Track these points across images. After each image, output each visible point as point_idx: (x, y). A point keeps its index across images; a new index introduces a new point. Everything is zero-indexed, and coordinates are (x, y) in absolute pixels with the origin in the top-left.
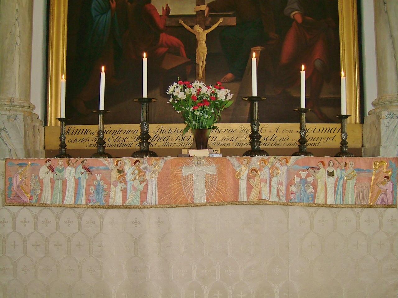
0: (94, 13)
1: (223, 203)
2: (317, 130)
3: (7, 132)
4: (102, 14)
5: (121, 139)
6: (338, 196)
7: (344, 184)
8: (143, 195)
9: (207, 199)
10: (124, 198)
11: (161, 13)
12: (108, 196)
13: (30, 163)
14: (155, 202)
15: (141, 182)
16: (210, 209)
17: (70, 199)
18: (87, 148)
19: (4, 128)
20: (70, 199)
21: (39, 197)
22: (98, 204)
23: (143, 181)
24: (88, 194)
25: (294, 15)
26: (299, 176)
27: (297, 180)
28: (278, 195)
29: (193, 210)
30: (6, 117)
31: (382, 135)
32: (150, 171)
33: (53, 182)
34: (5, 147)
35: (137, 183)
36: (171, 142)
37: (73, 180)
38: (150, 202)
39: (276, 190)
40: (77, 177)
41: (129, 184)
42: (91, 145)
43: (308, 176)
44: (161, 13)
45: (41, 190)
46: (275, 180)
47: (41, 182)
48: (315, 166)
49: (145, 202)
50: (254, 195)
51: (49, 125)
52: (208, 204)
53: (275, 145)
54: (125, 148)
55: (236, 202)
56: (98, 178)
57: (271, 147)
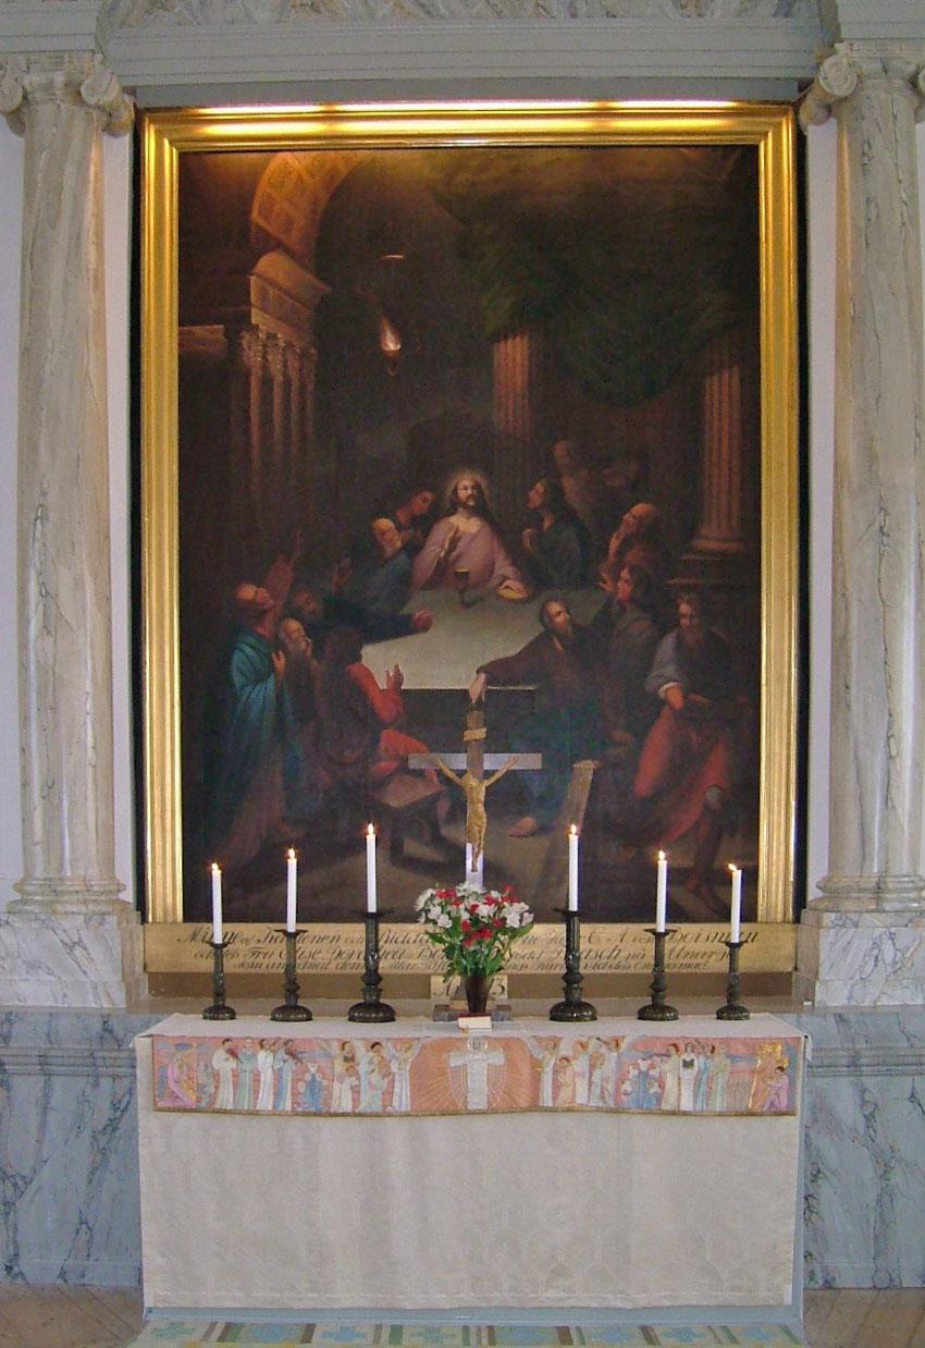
0: (238, 679)
1: (513, 1110)
2: (704, 937)
3: (85, 949)
4: (257, 683)
5: (307, 954)
6: (700, 1098)
7: (711, 1079)
8: (387, 1097)
9: (489, 1103)
10: (356, 1101)
11: (382, 685)
12: (330, 1096)
13: (195, 1045)
14: (405, 1106)
15: (384, 1076)
16: (491, 1119)
17: (265, 1102)
18: (237, 971)
19: (80, 941)
20: (265, 1102)
21: (213, 1098)
22: (313, 1109)
23: (387, 1074)
24: (295, 1094)
25: (668, 689)
26: (636, 1066)
27: (633, 1072)
28: (602, 1097)
29: (465, 1120)
30: (81, 918)
31: (821, 959)
32: (396, 1058)
33: (236, 1074)
34: (83, 978)
35: (375, 1078)
36: (407, 961)
37: (270, 1072)
38: (397, 1108)
39: (599, 1088)
40: (276, 1067)
41: (363, 1078)
42: (243, 965)
43: (652, 1067)
44: (382, 685)
45: (217, 1088)
46: (597, 1073)
47: (216, 1076)
48: (664, 1052)
49: (390, 1108)
50: (565, 1094)
51: (150, 919)
52: (491, 1111)
53: (618, 967)
54: (314, 971)
55: (535, 1107)
56: (313, 1070)
57: (609, 972)
